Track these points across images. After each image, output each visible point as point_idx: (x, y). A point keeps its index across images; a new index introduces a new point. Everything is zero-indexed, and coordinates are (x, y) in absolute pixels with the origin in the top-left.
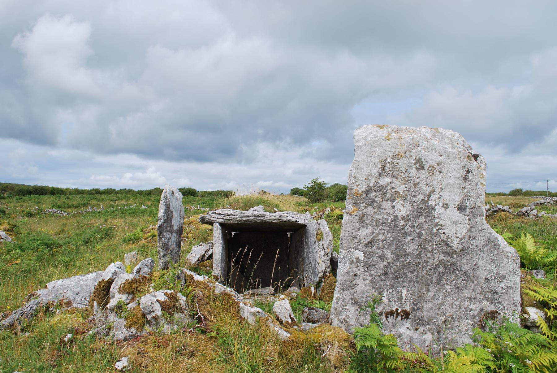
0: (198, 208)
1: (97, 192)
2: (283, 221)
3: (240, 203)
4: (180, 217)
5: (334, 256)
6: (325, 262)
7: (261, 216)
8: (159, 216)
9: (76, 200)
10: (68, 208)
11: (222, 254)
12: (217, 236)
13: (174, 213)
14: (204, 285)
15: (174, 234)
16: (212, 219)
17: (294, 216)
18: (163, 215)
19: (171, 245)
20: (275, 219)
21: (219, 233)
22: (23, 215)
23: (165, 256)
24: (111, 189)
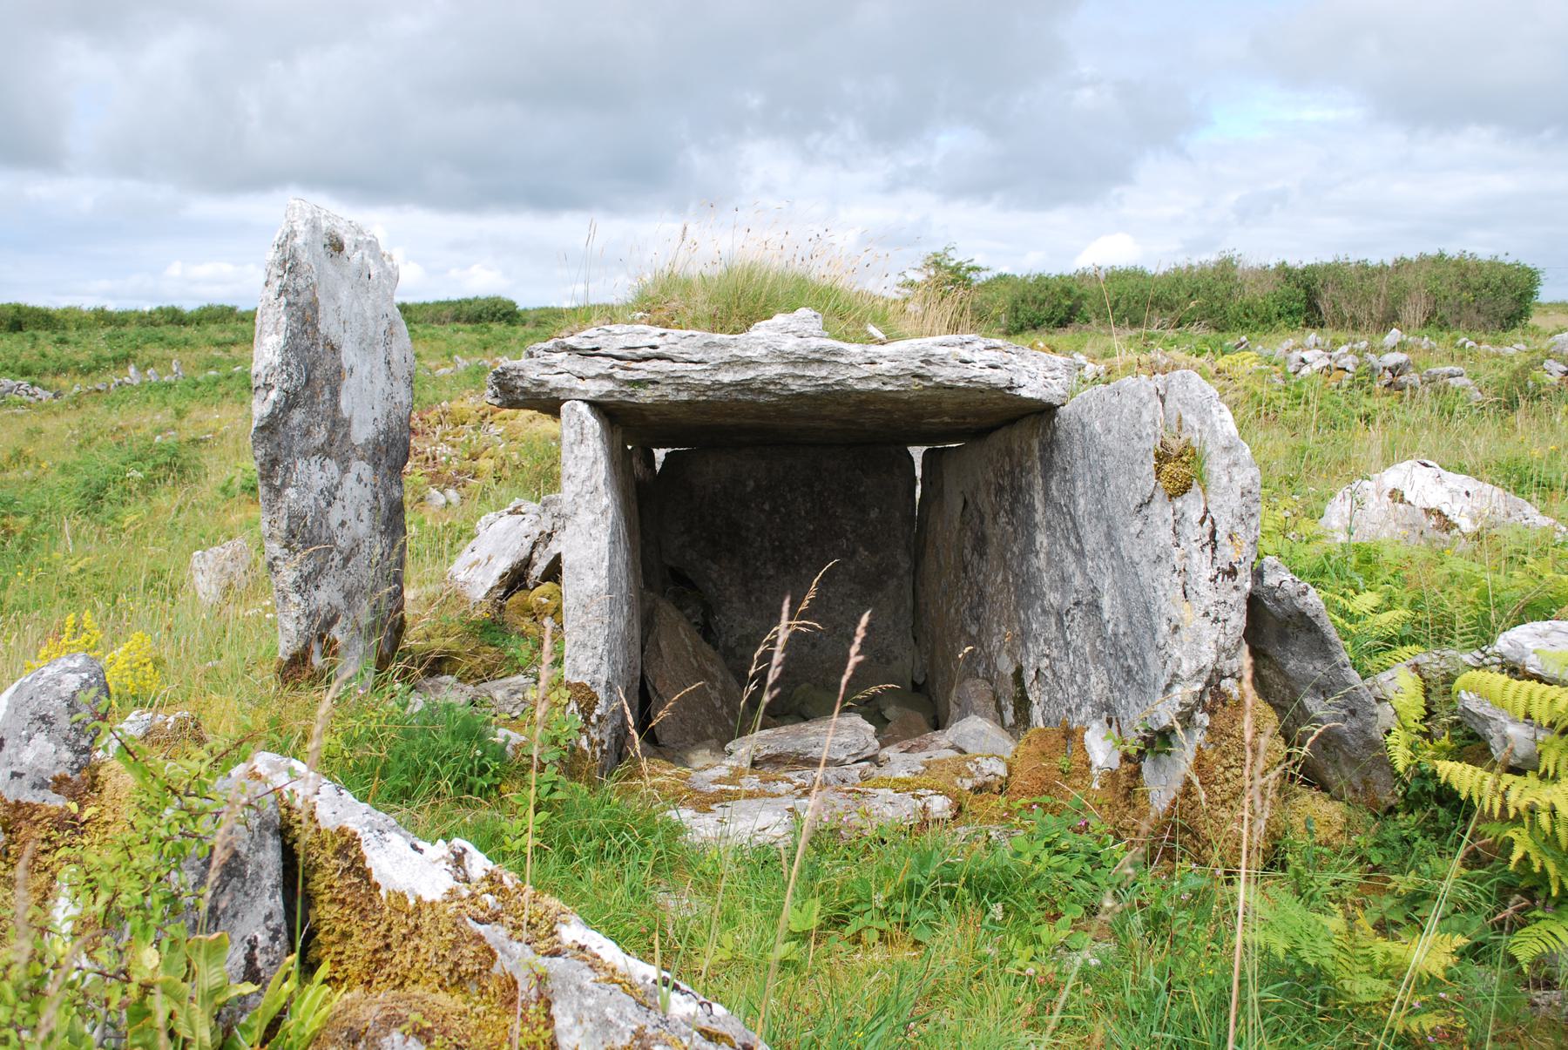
1: (175, 318)
2: (940, 386)
3: (700, 297)
4: (391, 376)
5: (1271, 580)
6: (1216, 620)
7: (820, 361)
8: (258, 367)
9: (98, 343)
10: (56, 374)
11: (611, 567)
12: (583, 474)
13: (349, 356)
14: (455, 945)
15: (361, 468)
16: (554, 381)
17: (993, 356)
18: (277, 360)
19: (343, 524)
20: (897, 377)
21: (591, 454)
23: (307, 582)
24: (222, 307)
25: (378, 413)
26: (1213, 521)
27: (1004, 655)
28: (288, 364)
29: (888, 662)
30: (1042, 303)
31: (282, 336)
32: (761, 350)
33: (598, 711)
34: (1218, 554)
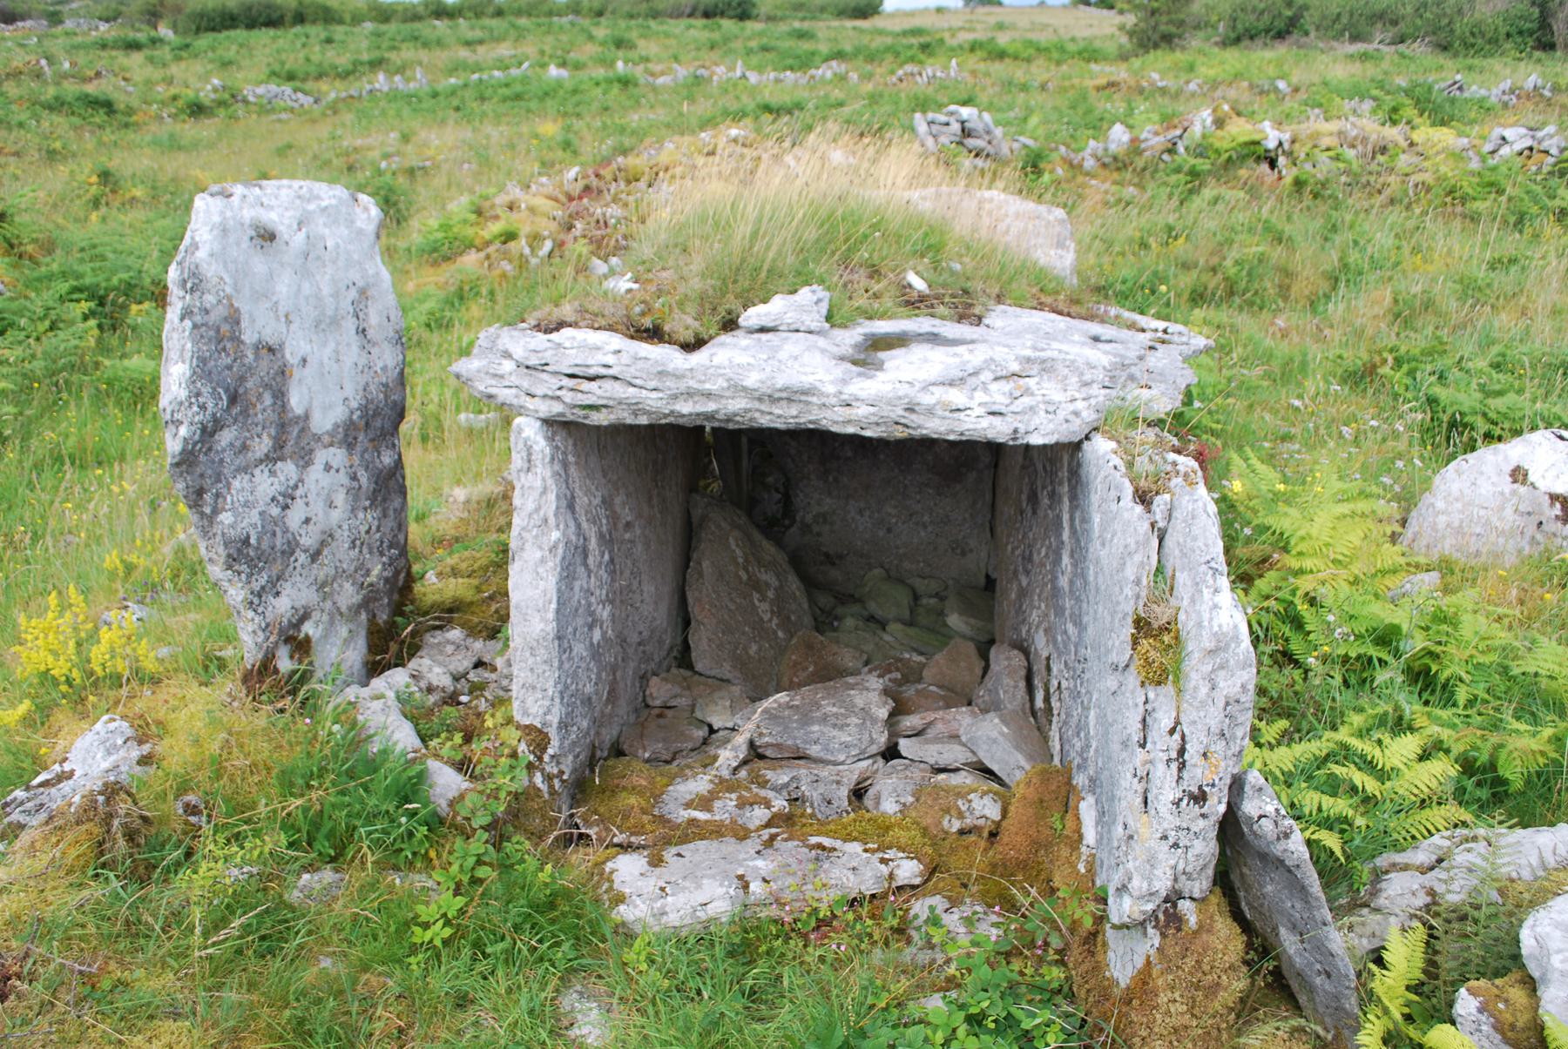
0: (738, 73)
6: (1176, 845)
12: (531, 506)
20: (877, 424)
21: (539, 483)
22: (173, 111)
25: (349, 391)
26: (1183, 737)
27: (1041, 632)
28: (198, 395)
29: (963, 554)
30: (1262, 13)
31: (187, 366)
32: (722, 383)
33: (550, 751)
34: (1185, 774)
